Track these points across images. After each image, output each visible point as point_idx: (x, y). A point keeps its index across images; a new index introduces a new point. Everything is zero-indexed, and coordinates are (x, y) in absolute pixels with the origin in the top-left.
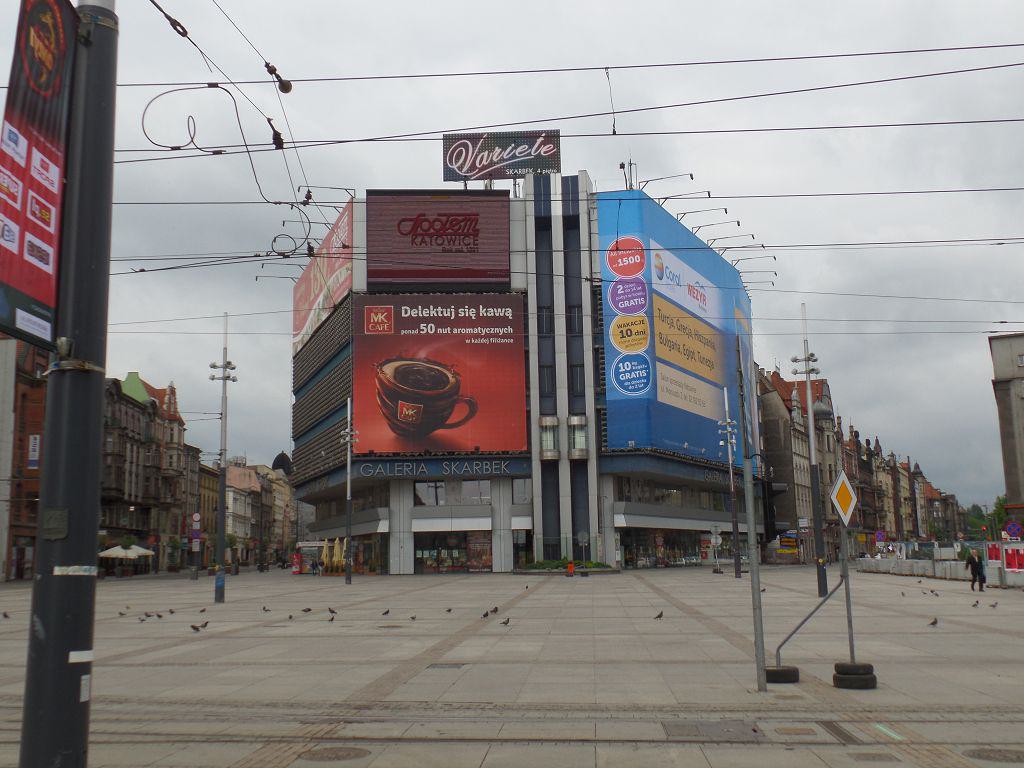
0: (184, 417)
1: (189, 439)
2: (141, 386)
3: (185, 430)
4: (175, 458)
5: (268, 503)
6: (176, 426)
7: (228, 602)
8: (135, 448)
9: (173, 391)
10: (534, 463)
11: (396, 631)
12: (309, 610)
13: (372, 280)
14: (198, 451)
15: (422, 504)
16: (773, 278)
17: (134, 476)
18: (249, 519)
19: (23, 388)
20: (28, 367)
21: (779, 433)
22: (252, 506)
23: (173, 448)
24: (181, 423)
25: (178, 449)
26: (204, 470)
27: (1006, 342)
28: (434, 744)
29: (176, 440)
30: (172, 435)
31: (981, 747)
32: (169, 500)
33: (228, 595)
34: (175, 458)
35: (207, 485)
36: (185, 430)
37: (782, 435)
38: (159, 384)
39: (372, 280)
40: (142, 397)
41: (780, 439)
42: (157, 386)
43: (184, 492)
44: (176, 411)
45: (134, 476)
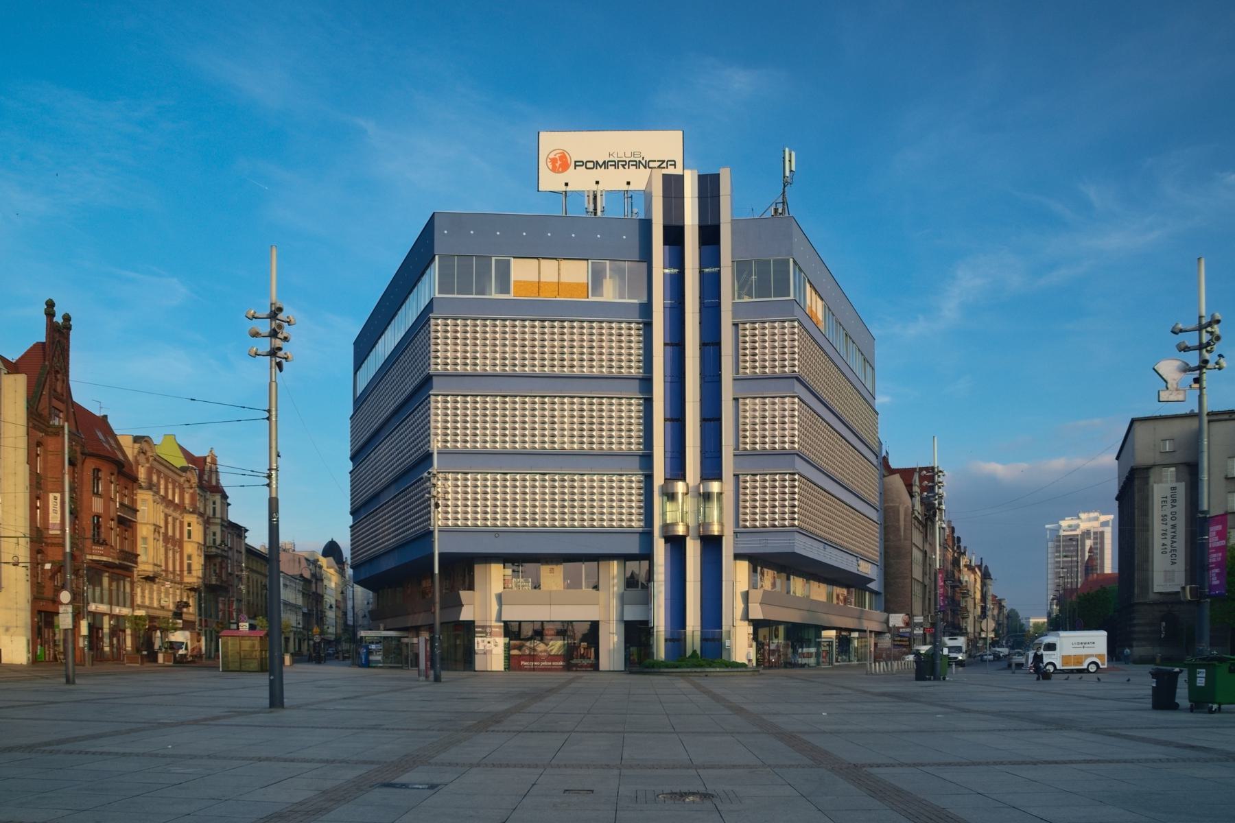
0: (228, 491)
1: (234, 516)
2: (178, 448)
3: (229, 504)
5: (321, 593)
6: (218, 498)
7: (292, 707)
11: (334, 689)
12: (592, 791)
13: (1068, 628)
17: (251, 592)
18: (300, 608)
21: (898, 520)
22: (303, 594)
24: (225, 497)
27: (1151, 424)
29: (218, 515)
30: (214, 509)
33: (289, 695)
36: (229, 504)
37: (902, 523)
39: (1068, 628)
41: (898, 529)
42: (197, 453)
43: (126, 539)
45: (251, 592)
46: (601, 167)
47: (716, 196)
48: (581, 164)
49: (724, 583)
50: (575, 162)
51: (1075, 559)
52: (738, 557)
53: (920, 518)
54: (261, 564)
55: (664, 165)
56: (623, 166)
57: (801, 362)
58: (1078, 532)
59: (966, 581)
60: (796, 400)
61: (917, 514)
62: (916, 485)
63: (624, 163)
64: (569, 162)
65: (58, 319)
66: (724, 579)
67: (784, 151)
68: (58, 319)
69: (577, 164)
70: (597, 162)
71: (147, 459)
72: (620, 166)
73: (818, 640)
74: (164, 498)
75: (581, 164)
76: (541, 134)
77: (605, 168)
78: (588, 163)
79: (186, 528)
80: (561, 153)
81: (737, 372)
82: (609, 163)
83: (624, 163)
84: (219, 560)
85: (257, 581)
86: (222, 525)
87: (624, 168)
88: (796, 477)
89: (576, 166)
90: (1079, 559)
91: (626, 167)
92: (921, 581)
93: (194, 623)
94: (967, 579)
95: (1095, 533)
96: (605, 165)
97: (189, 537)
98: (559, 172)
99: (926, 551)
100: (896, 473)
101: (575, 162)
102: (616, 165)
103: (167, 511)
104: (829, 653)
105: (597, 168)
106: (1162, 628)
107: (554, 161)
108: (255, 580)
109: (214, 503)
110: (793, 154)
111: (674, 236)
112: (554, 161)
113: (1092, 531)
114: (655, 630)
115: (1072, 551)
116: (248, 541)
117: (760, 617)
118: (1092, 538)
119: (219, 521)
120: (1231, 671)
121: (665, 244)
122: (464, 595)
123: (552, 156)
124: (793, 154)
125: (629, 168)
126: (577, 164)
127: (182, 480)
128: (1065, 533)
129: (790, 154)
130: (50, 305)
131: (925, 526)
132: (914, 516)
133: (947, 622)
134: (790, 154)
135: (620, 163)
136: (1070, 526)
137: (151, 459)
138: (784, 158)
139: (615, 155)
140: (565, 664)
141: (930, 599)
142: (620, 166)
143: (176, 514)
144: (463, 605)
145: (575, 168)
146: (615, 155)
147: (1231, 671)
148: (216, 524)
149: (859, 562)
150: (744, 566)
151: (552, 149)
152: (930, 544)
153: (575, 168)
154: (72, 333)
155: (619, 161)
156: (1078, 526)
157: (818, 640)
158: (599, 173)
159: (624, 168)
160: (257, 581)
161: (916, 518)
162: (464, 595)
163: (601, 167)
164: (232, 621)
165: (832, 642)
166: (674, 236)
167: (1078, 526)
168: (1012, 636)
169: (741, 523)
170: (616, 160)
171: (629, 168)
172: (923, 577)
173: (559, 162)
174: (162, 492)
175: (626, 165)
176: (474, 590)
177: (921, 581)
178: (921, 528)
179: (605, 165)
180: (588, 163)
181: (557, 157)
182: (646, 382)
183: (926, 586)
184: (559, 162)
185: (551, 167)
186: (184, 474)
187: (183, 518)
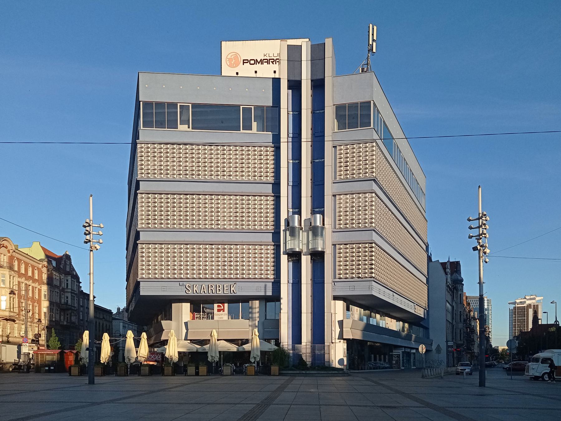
2: (41, 249)
22: (137, 331)
29: (69, 287)
30: (67, 284)
32: (65, 323)
38: (60, 253)
43: (82, 320)
46: (259, 63)
48: (247, 61)
49: (326, 314)
50: (244, 60)
51: (524, 318)
52: (336, 298)
53: (451, 287)
54: (99, 313)
56: (272, 62)
57: (377, 166)
58: (525, 305)
59: (473, 325)
60: (374, 195)
61: (448, 284)
62: (448, 268)
63: (273, 60)
64: (240, 61)
66: (326, 311)
67: (369, 27)
69: (245, 61)
70: (256, 60)
71: (9, 251)
72: (271, 63)
73: (391, 353)
74: (18, 272)
75: (247, 61)
76: (223, 42)
77: (261, 64)
78: (251, 61)
80: (235, 55)
81: (335, 178)
82: (264, 61)
83: (273, 60)
84: (70, 311)
85: (99, 323)
86: (71, 293)
87: (273, 64)
88: (374, 245)
89: (244, 63)
90: (526, 318)
91: (274, 63)
92: (451, 322)
94: (474, 325)
95: (534, 306)
96: (262, 62)
99: (453, 306)
100: (414, 349)
101: (244, 60)
102: (268, 62)
103: (20, 280)
104: (398, 362)
105: (256, 64)
107: (230, 60)
108: (98, 324)
109: (67, 281)
110: (375, 27)
112: (230, 60)
113: (532, 304)
114: (281, 345)
115: (521, 314)
117: (351, 337)
118: (532, 308)
119: (70, 290)
121: (289, 88)
122: (165, 323)
123: (229, 57)
124: (375, 27)
125: (276, 64)
126: (245, 61)
127: (40, 266)
128: (518, 306)
129: (373, 29)
131: (453, 292)
132: (447, 285)
134: (373, 29)
135: (271, 61)
136: (521, 302)
137: (11, 251)
138: (369, 32)
139: (267, 55)
142: (271, 63)
143: (36, 285)
144: (164, 330)
145: (243, 64)
146: (267, 55)
148: (68, 292)
149: (415, 307)
150: (340, 304)
151: (230, 52)
152: (455, 302)
153: (243, 64)
155: (270, 59)
156: (525, 302)
157: (391, 353)
158: (258, 67)
159: (273, 64)
160: (99, 323)
161: (448, 286)
162: (165, 323)
163: (259, 63)
164: (153, 351)
165: (400, 355)
167: (525, 302)
168: (494, 355)
169: (337, 276)
170: (268, 58)
171: (276, 64)
172: (452, 320)
173: (234, 61)
174: (16, 269)
175: (274, 62)
176: (171, 320)
177: (451, 322)
178: (451, 293)
179: (262, 62)
180: (251, 61)
181: (232, 57)
182: (276, 185)
183: (454, 325)
184: (234, 61)
186: (41, 263)
187: (41, 287)
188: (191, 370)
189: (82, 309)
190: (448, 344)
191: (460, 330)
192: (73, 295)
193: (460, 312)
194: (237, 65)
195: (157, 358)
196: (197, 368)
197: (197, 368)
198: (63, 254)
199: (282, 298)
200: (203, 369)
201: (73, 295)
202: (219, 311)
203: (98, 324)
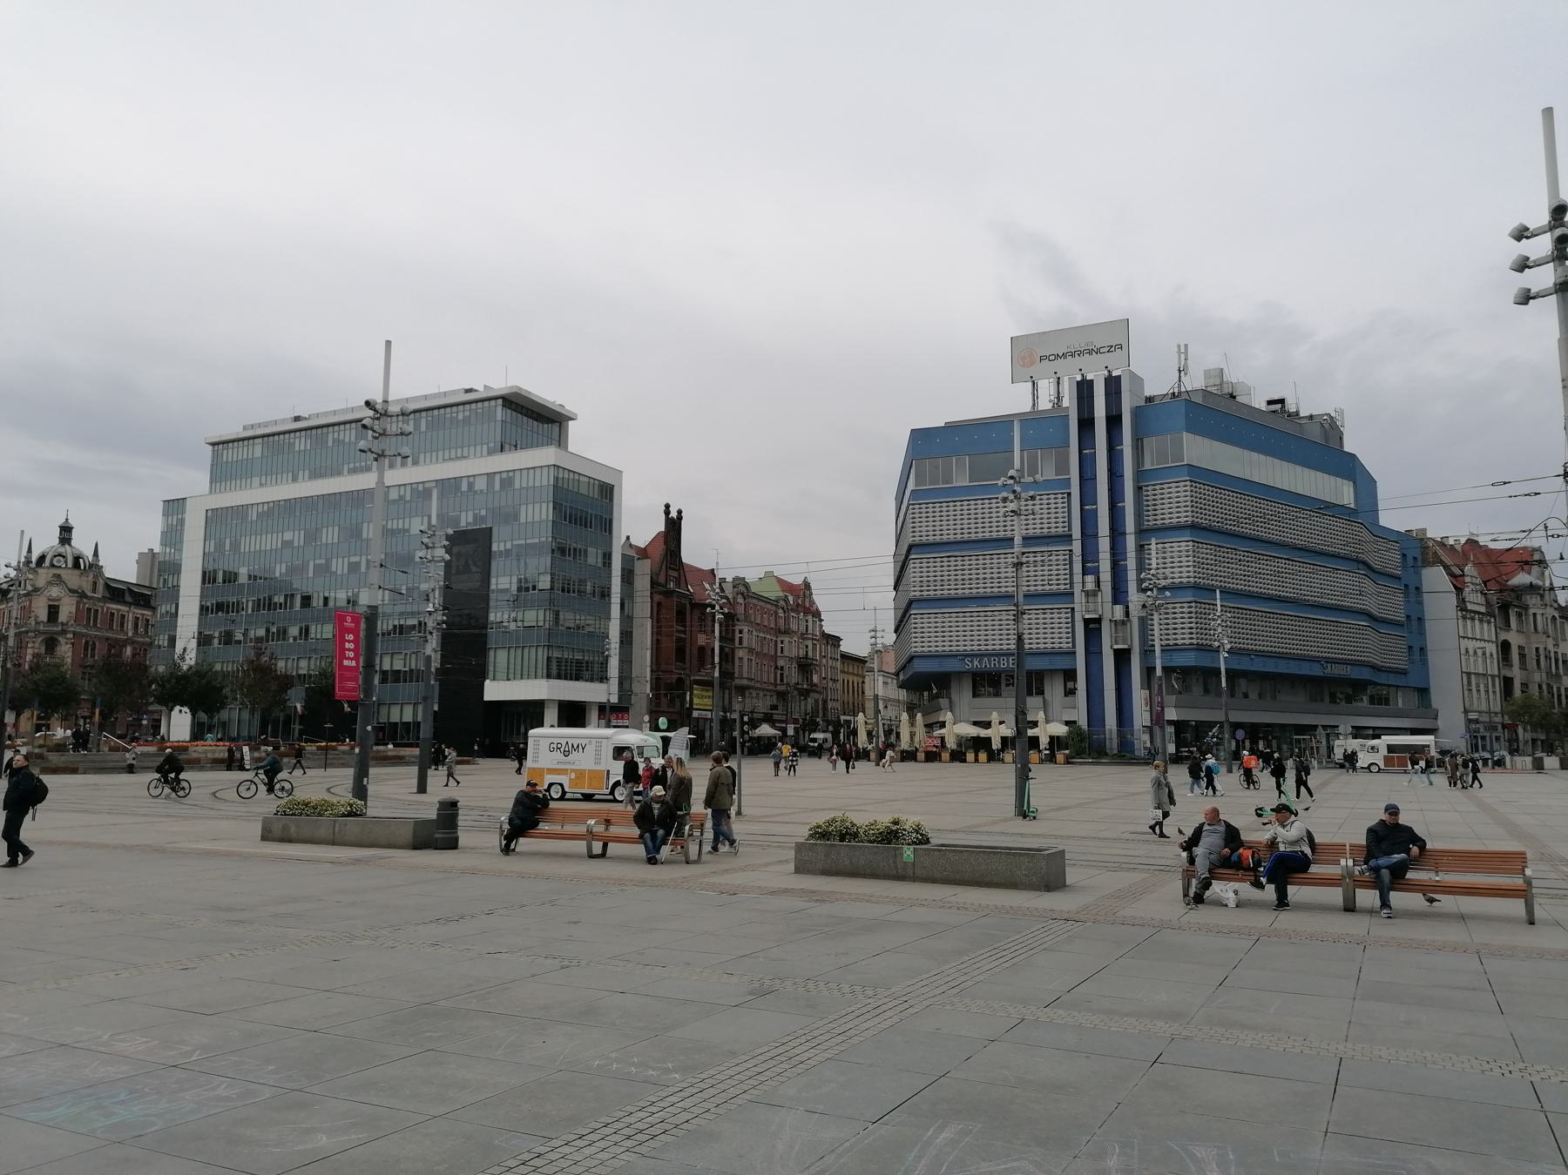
4: (810, 647)
8: (810, 654)
9: (807, 585)
10: (1103, 414)
14: (838, 639)
15: (1165, 836)
16: (1162, 637)
19: (657, 598)
20: (662, 579)
23: (808, 639)
25: (813, 639)
26: (846, 657)
28: (1210, 533)
29: (810, 631)
31: (1099, 761)
32: (805, 686)
34: (810, 647)
35: (851, 671)
38: (797, 580)
40: (774, 592)
43: (824, 678)
44: (812, 603)
47: (1119, 393)
55: (1113, 349)
56: (1079, 355)
65: (674, 514)
68: (674, 514)
72: (1077, 356)
79: (780, 645)
85: (848, 681)
93: (240, 641)
97: (782, 652)
98: (1028, 367)
106: (176, 656)
108: (846, 681)
111: (1086, 424)
116: (842, 648)
120: (1564, 766)
130: (667, 506)
133: (258, 659)
140: (439, 667)
141: (1494, 692)
142: (1077, 356)
147: (1564, 766)
154: (683, 521)
160: (848, 681)
166: (1086, 424)
185: (1021, 363)
188: (970, 756)
189: (824, 661)
190: (1470, 717)
191: (1540, 686)
192: (815, 642)
193: (1537, 649)
194: (1032, 363)
195: (935, 742)
196: (976, 756)
197: (976, 756)
198: (929, 824)
199: (1424, 531)
200: (983, 756)
201: (815, 642)
202: (1007, 685)
203: (846, 681)
